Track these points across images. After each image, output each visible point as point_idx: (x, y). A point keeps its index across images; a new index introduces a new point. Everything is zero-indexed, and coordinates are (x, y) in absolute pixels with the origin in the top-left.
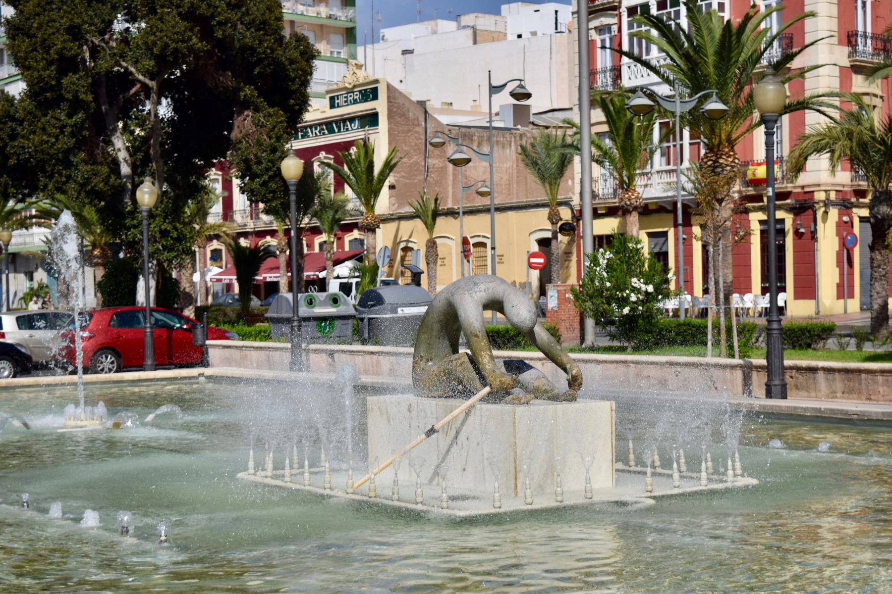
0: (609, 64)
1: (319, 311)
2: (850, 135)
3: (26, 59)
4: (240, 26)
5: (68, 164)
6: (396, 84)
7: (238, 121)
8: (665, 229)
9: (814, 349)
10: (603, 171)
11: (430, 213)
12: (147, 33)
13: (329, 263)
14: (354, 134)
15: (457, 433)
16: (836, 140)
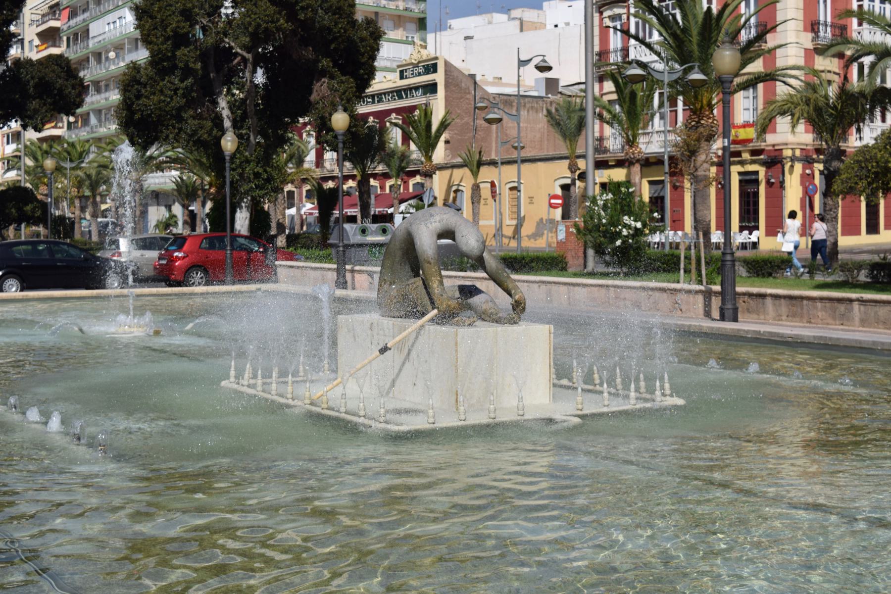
0: (619, 46)
1: (370, 239)
2: (807, 102)
3: (149, 35)
4: (320, 11)
5: (180, 119)
6: (456, 63)
7: (316, 86)
8: (663, 178)
9: (774, 277)
10: (614, 131)
11: (475, 163)
12: (244, 15)
13: (396, 202)
14: (418, 99)
15: (410, 351)
16: (796, 105)
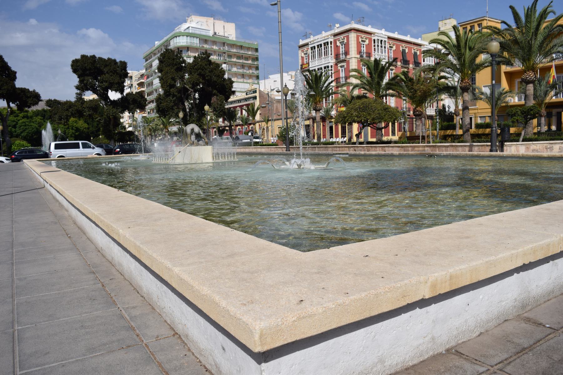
5: (173, 109)
7: (212, 99)
14: (251, 101)
